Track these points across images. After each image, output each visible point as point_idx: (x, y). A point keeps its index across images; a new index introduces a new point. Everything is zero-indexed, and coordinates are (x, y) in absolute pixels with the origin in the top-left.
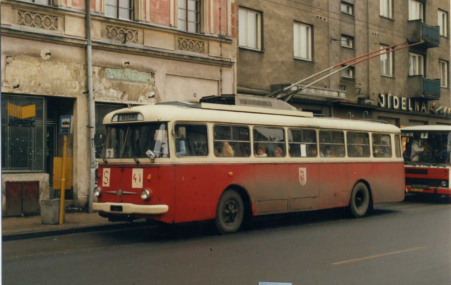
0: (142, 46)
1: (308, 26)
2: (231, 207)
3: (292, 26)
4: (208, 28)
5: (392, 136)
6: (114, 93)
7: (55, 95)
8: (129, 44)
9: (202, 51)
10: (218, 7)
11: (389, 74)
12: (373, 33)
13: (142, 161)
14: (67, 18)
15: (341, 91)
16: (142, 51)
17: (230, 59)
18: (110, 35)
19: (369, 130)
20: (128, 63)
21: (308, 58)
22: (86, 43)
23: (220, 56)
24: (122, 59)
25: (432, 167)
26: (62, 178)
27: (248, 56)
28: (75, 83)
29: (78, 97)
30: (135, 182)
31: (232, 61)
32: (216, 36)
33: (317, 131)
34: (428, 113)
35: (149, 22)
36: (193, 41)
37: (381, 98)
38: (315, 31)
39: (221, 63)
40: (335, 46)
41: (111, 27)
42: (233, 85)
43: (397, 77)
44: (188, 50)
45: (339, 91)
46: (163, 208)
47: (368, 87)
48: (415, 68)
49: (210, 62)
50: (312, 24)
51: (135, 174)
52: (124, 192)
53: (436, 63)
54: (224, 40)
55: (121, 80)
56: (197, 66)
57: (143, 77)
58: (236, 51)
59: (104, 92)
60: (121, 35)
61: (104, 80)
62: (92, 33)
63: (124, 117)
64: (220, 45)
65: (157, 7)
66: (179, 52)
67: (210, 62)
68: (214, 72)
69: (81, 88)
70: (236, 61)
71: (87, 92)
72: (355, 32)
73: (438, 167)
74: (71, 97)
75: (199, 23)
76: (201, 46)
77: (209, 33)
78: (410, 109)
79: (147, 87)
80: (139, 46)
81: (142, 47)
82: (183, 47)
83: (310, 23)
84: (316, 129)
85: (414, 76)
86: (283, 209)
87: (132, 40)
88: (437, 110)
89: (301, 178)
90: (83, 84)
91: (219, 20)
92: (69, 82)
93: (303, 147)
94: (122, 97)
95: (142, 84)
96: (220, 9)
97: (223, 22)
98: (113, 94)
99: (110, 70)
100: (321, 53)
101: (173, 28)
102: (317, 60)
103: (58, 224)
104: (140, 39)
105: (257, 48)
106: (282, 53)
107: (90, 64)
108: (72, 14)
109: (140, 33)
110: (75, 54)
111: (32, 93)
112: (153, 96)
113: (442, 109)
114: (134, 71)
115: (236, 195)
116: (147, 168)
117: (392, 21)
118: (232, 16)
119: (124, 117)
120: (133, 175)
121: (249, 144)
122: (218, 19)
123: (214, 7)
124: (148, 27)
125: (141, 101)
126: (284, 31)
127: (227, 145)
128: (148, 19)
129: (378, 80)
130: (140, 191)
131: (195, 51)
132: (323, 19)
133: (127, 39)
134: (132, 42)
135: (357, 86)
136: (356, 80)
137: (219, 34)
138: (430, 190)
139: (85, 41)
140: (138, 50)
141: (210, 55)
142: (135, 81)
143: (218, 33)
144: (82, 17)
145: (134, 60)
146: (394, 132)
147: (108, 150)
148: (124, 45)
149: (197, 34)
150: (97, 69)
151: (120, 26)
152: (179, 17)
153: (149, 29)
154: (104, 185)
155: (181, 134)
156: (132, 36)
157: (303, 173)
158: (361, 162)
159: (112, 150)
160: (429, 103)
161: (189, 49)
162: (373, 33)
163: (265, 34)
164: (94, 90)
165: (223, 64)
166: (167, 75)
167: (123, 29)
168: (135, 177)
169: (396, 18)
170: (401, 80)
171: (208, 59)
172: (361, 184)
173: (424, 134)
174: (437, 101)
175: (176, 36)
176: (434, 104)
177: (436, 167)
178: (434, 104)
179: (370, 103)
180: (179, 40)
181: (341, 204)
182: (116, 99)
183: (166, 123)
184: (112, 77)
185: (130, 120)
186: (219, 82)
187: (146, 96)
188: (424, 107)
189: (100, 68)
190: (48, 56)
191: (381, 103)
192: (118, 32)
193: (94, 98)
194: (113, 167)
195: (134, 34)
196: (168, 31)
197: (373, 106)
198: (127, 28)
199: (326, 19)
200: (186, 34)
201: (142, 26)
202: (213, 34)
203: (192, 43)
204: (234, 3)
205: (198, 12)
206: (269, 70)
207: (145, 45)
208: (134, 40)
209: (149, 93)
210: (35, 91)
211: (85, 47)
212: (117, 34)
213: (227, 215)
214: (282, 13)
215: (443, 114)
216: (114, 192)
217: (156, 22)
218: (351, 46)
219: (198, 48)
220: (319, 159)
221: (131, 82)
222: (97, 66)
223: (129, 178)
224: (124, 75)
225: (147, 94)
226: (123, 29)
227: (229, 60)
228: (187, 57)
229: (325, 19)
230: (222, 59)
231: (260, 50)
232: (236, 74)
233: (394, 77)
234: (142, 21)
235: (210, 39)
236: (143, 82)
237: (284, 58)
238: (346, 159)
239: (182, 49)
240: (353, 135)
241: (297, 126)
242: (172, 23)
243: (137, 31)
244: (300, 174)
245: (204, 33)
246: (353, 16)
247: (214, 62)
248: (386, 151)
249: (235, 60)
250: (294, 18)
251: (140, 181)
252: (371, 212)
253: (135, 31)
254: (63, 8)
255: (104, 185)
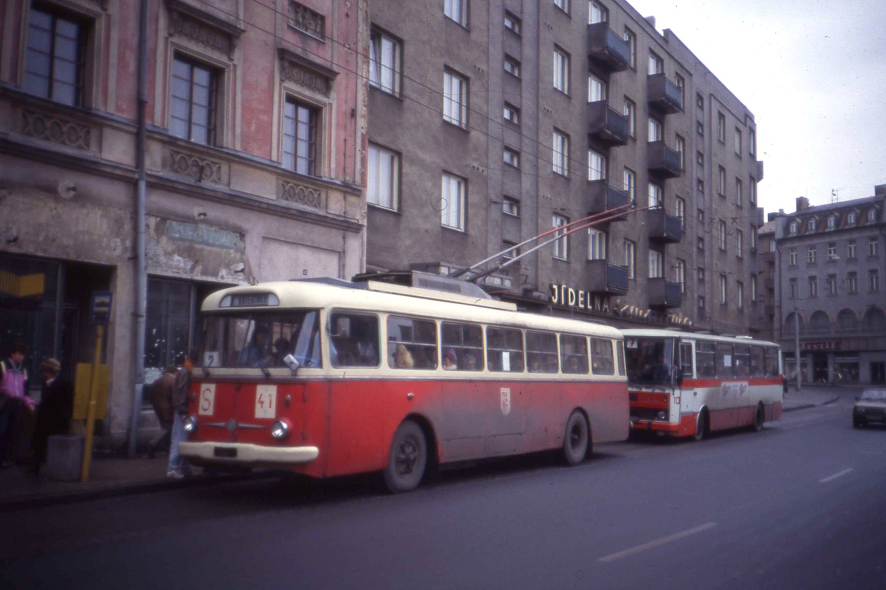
0: (227, 188)
1: (460, 180)
2: (409, 450)
3: (440, 179)
4: (326, 170)
5: (614, 344)
6: (179, 261)
7: (80, 260)
8: (207, 184)
9: (318, 205)
10: (342, 137)
11: (562, 257)
12: (544, 196)
13: (276, 372)
14: (107, 132)
15: (506, 277)
16: (226, 197)
17: (358, 220)
18: (176, 166)
19: (587, 333)
20: (205, 214)
21: (459, 227)
22: (136, 176)
23: (343, 215)
24: (195, 209)
25: (644, 390)
26: (90, 399)
27: (379, 219)
28: (116, 242)
29: (119, 264)
30: (262, 407)
31: (360, 222)
32: (338, 182)
33: (524, 332)
34: (610, 314)
35: (239, 151)
36: (305, 187)
37: (553, 290)
38: (470, 188)
39: (345, 224)
40: (494, 214)
41: (179, 153)
42: (361, 260)
43: (573, 261)
44: (297, 201)
45: (502, 276)
46: (313, 450)
47: (536, 275)
48: (595, 251)
49: (328, 223)
50: (466, 177)
51: (261, 395)
52: (241, 425)
53: (620, 244)
54: (350, 190)
55: (192, 241)
56: (309, 227)
57: (226, 239)
58: (365, 209)
59: (163, 259)
60: (194, 169)
61: (164, 240)
62: (147, 162)
63: (242, 301)
64: (345, 198)
65: (253, 128)
66: (284, 203)
67: (328, 223)
68: (333, 237)
69: (125, 250)
70: (365, 224)
71: (135, 258)
72: (520, 193)
73: (653, 390)
74: (107, 263)
75: (314, 159)
76: (316, 196)
77: (596, 169)
78: (589, 307)
79: (232, 256)
80: (221, 188)
81: (226, 190)
82: (290, 196)
83: (463, 176)
84: (522, 330)
85: (594, 261)
86: (479, 453)
87: (211, 179)
88: (622, 310)
89: (504, 403)
90: (128, 243)
91: (343, 158)
92: (105, 240)
93: (506, 356)
94: (192, 269)
95: (225, 250)
96: (345, 140)
97: (349, 162)
98: (178, 264)
99: (174, 223)
100: (477, 222)
101: (276, 165)
102: (472, 232)
103: (79, 479)
104: (224, 177)
105: (391, 206)
106: (426, 218)
107: (142, 212)
108: (116, 126)
109: (225, 168)
110: (116, 192)
111: (40, 254)
112: (242, 271)
113: (628, 309)
114: (213, 229)
115: (414, 429)
116: (283, 385)
117: (568, 180)
118: (362, 153)
119: (242, 301)
120: (258, 396)
121: (434, 349)
122: (342, 156)
123: (337, 138)
124: (237, 159)
125: (222, 277)
126: (429, 184)
127: (404, 350)
128: (238, 147)
129: (550, 265)
130: (271, 424)
131: (307, 204)
132: (480, 171)
133: (203, 176)
134: (211, 181)
135: (523, 271)
136: (521, 263)
137: (343, 180)
138: (642, 424)
139: (136, 172)
140: (220, 195)
141: (329, 211)
142: (213, 245)
143: (341, 178)
144: (127, 132)
145: (216, 212)
146: (616, 337)
147: (207, 354)
148: (199, 184)
149: (310, 176)
150: (153, 221)
151: (193, 154)
152: (285, 149)
153: (238, 163)
154: (201, 412)
155: (343, 329)
156: (212, 173)
157: (506, 395)
158: (501, 379)
159: (216, 355)
160: (612, 299)
161: (299, 201)
162: (544, 196)
163: (404, 187)
164: (146, 255)
165: (348, 227)
166: (264, 238)
167: (197, 159)
168: (261, 400)
169: (573, 177)
170: (577, 266)
171: (326, 217)
172: (578, 415)
173: (631, 342)
174: (622, 297)
175: (279, 177)
176: (618, 301)
177: (650, 391)
178: (618, 301)
179: (540, 296)
180: (284, 184)
181: (553, 444)
182: (183, 272)
183: (317, 311)
184: (177, 235)
185: (253, 304)
186: (342, 255)
187: (230, 270)
188: (606, 304)
189: (158, 219)
190: (72, 193)
191: (553, 297)
192: (190, 162)
193: (146, 268)
194: (221, 382)
195: (215, 169)
196: (268, 168)
197: (543, 301)
198: (205, 157)
199: (484, 171)
200: (294, 175)
201: (228, 157)
202: (333, 179)
203: (303, 191)
204: (365, 133)
205: (312, 142)
206: (408, 242)
207: (231, 188)
208: (214, 179)
209: (236, 265)
210: (45, 251)
211: (133, 184)
212: (187, 166)
213: (403, 462)
214: (427, 157)
215: (629, 315)
216: (222, 424)
217: (250, 151)
218: (515, 214)
219: (302, 197)
220: (525, 375)
221: (207, 245)
222: (153, 215)
223: (250, 402)
224: (196, 234)
225: (233, 267)
226: (197, 159)
227: (356, 222)
228: (295, 212)
229: (483, 171)
230: (347, 219)
231: (396, 211)
232: (365, 243)
233: (569, 261)
234: (227, 148)
235: (329, 186)
236: (229, 248)
237: (428, 226)
238: (560, 375)
239: (288, 200)
240: (576, 341)
241: (498, 323)
242: (274, 158)
243: (220, 164)
244: (502, 398)
245: (321, 177)
246: (518, 170)
247: (334, 222)
248: (604, 366)
249: (365, 222)
250: (443, 165)
251: (270, 406)
252: (590, 456)
253: (216, 163)
254: (101, 113)
255: (201, 412)
